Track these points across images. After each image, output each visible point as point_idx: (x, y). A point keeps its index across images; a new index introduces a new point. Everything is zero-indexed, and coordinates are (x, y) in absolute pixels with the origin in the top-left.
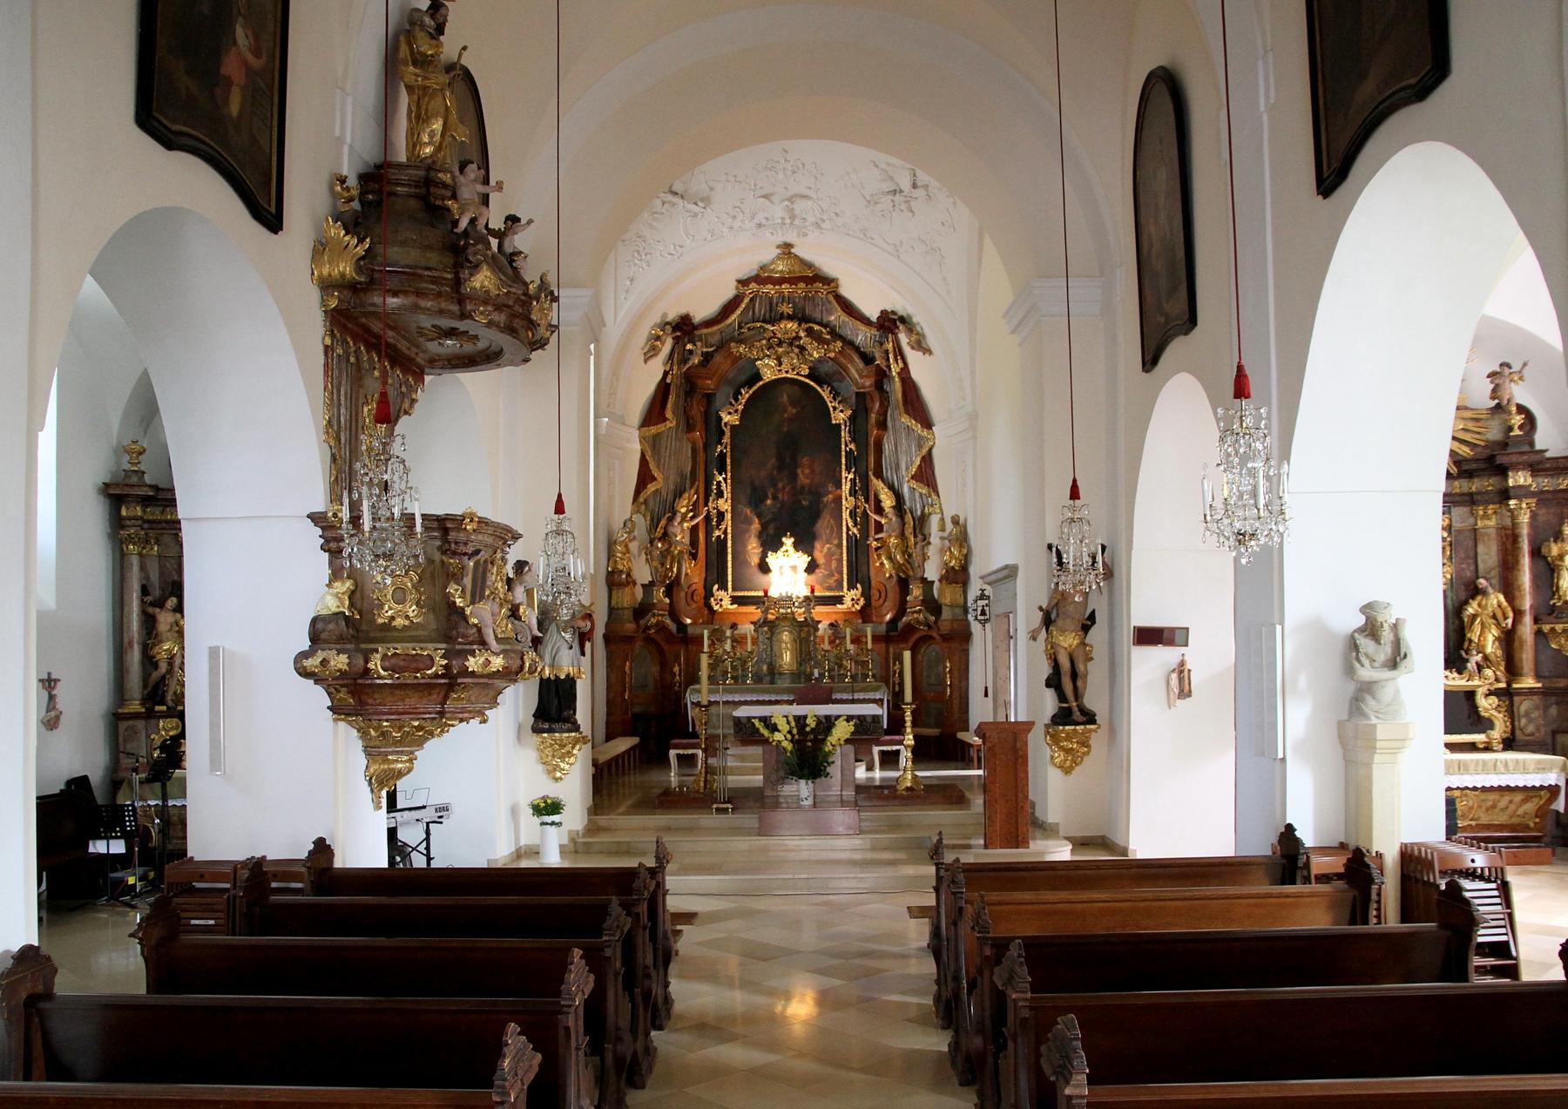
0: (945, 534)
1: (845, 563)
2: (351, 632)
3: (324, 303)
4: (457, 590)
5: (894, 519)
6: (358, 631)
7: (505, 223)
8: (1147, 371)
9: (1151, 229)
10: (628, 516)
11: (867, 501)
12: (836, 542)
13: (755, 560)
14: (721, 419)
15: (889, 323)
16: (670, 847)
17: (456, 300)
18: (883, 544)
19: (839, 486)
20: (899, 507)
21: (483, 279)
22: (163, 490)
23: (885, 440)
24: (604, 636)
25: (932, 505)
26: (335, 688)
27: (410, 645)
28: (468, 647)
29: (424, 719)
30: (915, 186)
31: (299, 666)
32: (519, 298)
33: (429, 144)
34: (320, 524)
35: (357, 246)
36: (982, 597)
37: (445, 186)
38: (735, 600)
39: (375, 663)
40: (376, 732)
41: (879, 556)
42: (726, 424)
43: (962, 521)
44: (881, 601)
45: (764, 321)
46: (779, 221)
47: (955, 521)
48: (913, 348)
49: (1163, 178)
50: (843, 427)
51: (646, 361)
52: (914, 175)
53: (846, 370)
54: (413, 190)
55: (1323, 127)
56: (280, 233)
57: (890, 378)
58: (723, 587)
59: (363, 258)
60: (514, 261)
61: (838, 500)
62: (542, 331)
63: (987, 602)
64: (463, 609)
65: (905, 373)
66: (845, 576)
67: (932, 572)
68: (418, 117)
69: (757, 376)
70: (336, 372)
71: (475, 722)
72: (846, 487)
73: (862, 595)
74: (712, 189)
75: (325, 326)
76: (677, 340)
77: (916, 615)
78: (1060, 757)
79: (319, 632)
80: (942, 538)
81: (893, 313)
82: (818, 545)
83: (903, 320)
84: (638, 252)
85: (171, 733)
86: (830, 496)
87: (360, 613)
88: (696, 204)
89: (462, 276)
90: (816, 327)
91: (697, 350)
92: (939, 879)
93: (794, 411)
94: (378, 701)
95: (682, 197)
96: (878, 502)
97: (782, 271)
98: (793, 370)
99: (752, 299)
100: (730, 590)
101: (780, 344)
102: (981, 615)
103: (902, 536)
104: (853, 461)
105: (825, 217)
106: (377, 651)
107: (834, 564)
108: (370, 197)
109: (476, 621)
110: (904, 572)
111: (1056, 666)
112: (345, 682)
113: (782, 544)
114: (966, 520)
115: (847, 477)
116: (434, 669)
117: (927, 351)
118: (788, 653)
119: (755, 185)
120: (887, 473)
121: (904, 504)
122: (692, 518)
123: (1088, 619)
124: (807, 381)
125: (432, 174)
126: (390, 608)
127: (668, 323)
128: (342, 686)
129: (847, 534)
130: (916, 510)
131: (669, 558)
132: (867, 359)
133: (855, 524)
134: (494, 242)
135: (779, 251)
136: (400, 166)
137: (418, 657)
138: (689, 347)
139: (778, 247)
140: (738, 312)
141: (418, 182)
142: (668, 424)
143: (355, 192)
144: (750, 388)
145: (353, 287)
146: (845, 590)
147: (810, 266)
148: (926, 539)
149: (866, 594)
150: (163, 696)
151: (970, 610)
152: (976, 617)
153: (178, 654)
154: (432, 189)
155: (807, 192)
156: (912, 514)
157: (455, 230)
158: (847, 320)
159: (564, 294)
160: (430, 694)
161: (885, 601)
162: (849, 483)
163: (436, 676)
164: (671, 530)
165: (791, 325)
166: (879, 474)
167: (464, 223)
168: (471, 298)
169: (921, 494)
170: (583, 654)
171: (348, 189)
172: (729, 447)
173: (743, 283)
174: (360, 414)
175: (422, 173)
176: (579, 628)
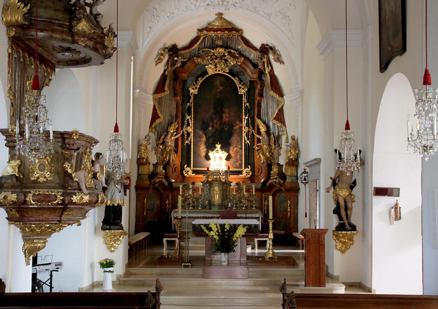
0: (289, 144)
1: (243, 156)
3: (8, 34)
4: (68, 166)
5: (266, 137)
6: (22, 183)
10: (147, 134)
11: (254, 129)
12: (239, 147)
13: (203, 154)
14: (189, 91)
17: (70, 35)
18: (260, 148)
19: (241, 122)
20: (268, 132)
25: (283, 131)
26: (10, 209)
28: (73, 191)
34: (5, 134)
35: (24, 8)
36: (305, 172)
38: (194, 172)
39: (30, 198)
41: (259, 153)
42: (191, 93)
43: (296, 138)
44: (259, 173)
45: (209, 48)
46: (217, 3)
47: (293, 138)
48: (275, 61)
50: (244, 96)
53: (245, 70)
57: (265, 74)
58: (189, 166)
59: (26, 13)
60: (97, 18)
61: (241, 128)
62: (110, 51)
63: (307, 174)
64: (71, 174)
66: (243, 162)
67: (282, 161)
69: (206, 73)
71: (75, 225)
72: (244, 123)
73: (251, 170)
75: (9, 44)
76: (170, 55)
78: (339, 245)
80: (287, 146)
81: (267, 45)
82: (231, 148)
83: (271, 48)
84: (154, 15)
86: (237, 126)
87: (23, 175)
89: (73, 24)
90: (233, 51)
91: (179, 61)
93: (222, 88)
96: (259, 129)
97: (218, 26)
98: (222, 70)
99: (204, 38)
100: (192, 167)
103: (269, 145)
104: (248, 111)
106: (30, 192)
107: (238, 157)
109: (77, 180)
110: (269, 161)
111: (338, 204)
112: (15, 206)
113: (216, 147)
115: (245, 118)
116: (57, 201)
117: (282, 62)
120: (263, 117)
121: (270, 130)
122: (176, 135)
123: (352, 183)
124: (228, 75)
126: (37, 173)
127: (166, 48)
128: (13, 208)
129: (245, 143)
130: (276, 133)
131: (165, 152)
132: (255, 66)
133: (248, 139)
134: (88, 9)
135: (216, 16)
138: (176, 59)
139: (216, 15)
140: (198, 43)
142: (166, 93)
144: (202, 78)
146: (243, 168)
148: (280, 146)
149: (253, 170)
151: (299, 178)
152: (302, 181)
156: (274, 135)
157: (70, 3)
160: (55, 212)
162: (246, 121)
163: (58, 204)
164: (166, 140)
165: (221, 50)
166: (259, 117)
169: (278, 126)
170: (125, 195)
172: (193, 104)
173: (200, 30)
176: (124, 183)
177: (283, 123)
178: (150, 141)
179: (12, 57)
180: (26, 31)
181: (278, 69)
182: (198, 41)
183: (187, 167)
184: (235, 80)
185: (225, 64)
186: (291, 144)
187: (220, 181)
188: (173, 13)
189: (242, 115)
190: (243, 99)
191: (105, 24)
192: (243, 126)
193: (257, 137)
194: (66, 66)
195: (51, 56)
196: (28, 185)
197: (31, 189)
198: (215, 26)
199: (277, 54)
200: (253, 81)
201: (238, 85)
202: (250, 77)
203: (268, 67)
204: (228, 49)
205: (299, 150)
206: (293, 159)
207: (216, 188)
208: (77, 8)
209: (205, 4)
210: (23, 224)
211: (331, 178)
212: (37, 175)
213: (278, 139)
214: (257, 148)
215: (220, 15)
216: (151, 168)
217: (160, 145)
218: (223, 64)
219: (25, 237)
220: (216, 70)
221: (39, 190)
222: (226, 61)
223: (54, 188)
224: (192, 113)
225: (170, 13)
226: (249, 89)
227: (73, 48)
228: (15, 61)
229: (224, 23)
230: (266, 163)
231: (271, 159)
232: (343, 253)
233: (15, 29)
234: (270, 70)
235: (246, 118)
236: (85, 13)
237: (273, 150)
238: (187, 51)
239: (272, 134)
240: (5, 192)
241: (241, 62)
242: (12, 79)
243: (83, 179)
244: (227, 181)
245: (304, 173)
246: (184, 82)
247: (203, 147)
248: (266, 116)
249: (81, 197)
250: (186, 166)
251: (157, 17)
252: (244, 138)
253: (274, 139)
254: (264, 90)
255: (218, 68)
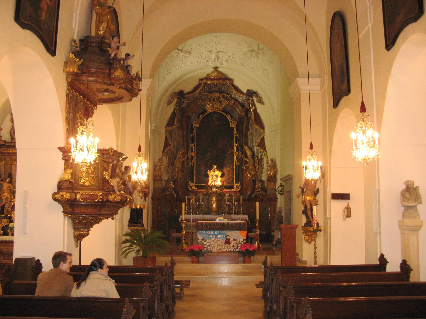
0: (269, 165)
2: (71, 186)
3: (67, 80)
4: (106, 174)
5: (251, 160)
6: (73, 186)
7: (125, 56)
8: (335, 108)
9: (335, 62)
10: (161, 157)
11: (242, 153)
13: (203, 173)
14: (193, 125)
15: (251, 93)
16: (175, 260)
17: (109, 80)
18: (248, 168)
19: (233, 148)
20: (253, 156)
21: (118, 73)
22: (7, 142)
23: (248, 133)
24: (152, 197)
25: (264, 155)
26: (65, 205)
27: (89, 191)
28: (109, 193)
29: (94, 217)
30: (259, 49)
31: (53, 197)
32: (129, 80)
33: (102, 30)
34: (62, 151)
35: (78, 62)
36: (281, 186)
37: (107, 43)
38: (196, 187)
39: (78, 196)
40: (78, 221)
41: (246, 172)
42: (194, 127)
43: (274, 160)
44: (247, 187)
45: (208, 93)
46: (214, 59)
47: (272, 160)
48: (258, 102)
49: (338, 46)
50: (234, 128)
51: (168, 105)
52: (259, 45)
53: (236, 110)
54: (97, 45)
55: (387, 30)
56: (55, 56)
57: (250, 112)
58: (193, 182)
59: (80, 65)
60: (128, 68)
62: (136, 91)
63: (283, 187)
64: (108, 180)
65: (255, 111)
67: (264, 177)
68: (99, 22)
69: (205, 111)
70: (69, 102)
71: (110, 219)
72: (235, 149)
73: (240, 185)
74: (191, 49)
75: (67, 87)
76: (178, 98)
77: (258, 192)
78: (307, 237)
79: (61, 186)
80: (267, 166)
81: (251, 90)
83: (255, 93)
84: (166, 69)
85: (6, 224)
87: (74, 180)
88: (186, 53)
89: (112, 72)
90: (226, 95)
91: (185, 101)
92: (266, 272)
93: (218, 123)
94: (79, 210)
95: (181, 51)
96: (246, 153)
97: (214, 76)
98: (218, 109)
99: (204, 85)
100: (195, 183)
101: (214, 100)
102: (281, 192)
103: (254, 165)
104: (237, 140)
105: (229, 58)
106: (79, 193)
107: (231, 175)
108: (83, 47)
109: (112, 184)
110: (254, 178)
111: (305, 206)
112: (69, 203)
113: (213, 167)
114: (276, 160)
115: (235, 145)
116: (98, 199)
117: (263, 103)
118: (215, 204)
119: (206, 48)
120: (249, 144)
121: (255, 154)
122: (182, 158)
123: (316, 191)
124: (222, 113)
125: (103, 39)
126: (84, 179)
127: (176, 93)
128: (67, 204)
130: (259, 157)
131: (174, 171)
132: (243, 106)
133: (238, 161)
134: (122, 62)
135: (213, 69)
136: (93, 37)
137: (93, 195)
138: (183, 101)
139: (213, 68)
140: (199, 89)
141: (98, 42)
142: (175, 127)
143: (78, 45)
144: (203, 115)
145: (76, 74)
146: (234, 184)
147: (224, 75)
148: (262, 167)
149: (242, 185)
150: (3, 211)
151: (277, 190)
152: (279, 193)
153: (9, 198)
154: (103, 45)
155: (223, 50)
156: (257, 158)
157: (110, 57)
158: (236, 92)
159: (143, 80)
160: (96, 208)
161: (248, 187)
162: (236, 148)
163: (98, 202)
164: (175, 162)
165: (217, 95)
166: (246, 145)
167: (113, 55)
168: (113, 78)
169: (260, 151)
170: (146, 201)
171: (76, 44)
172: (195, 134)
173: (201, 80)
174: (76, 116)
175: (100, 39)
176: (144, 192)
177: (265, 149)
178: (163, 163)
179: (69, 96)
180: (79, 77)
181: (260, 108)
182: (199, 87)
183: (191, 183)
184: (228, 116)
185: (220, 105)
186: (270, 165)
187: (217, 193)
188: (181, 67)
189: (233, 143)
190: (234, 131)
191: (134, 72)
192: (234, 151)
193: (245, 160)
194: (104, 103)
195: (94, 96)
196: (78, 187)
197: (80, 190)
198: (212, 77)
199: (259, 97)
200: (242, 117)
201: (230, 120)
202: (239, 114)
203: (253, 107)
204: (222, 94)
205: (277, 169)
206: (273, 176)
207: (214, 199)
208: (115, 61)
209: (205, 61)
210: (74, 216)
211: (300, 187)
212: (84, 181)
213: (261, 160)
214: (244, 168)
215: (216, 68)
216: (164, 183)
217: (170, 166)
218: (218, 105)
219: (75, 227)
220: (213, 109)
221: (85, 191)
222: (221, 102)
223: (96, 190)
224: (195, 142)
225: (179, 67)
226: (238, 123)
227: (110, 89)
228: (71, 99)
229: (219, 74)
230: (252, 180)
231: (256, 177)
232: (309, 243)
233: (72, 76)
234: (254, 109)
235: (236, 145)
236: (120, 65)
237: (257, 170)
238: (192, 95)
239: (256, 157)
240: (62, 192)
241: (232, 103)
242: (68, 112)
243: (116, 184)
244: (222, 193)
245: (280, 187)
246: (189, 118)
247: (203, 168)
248: (251, 143)
249: (115, 197)
250: (190, 182)
251: (169, 70)
252: (235, 160)
253: (257, 161)
254: (250, 124)
255: (214, 108)
